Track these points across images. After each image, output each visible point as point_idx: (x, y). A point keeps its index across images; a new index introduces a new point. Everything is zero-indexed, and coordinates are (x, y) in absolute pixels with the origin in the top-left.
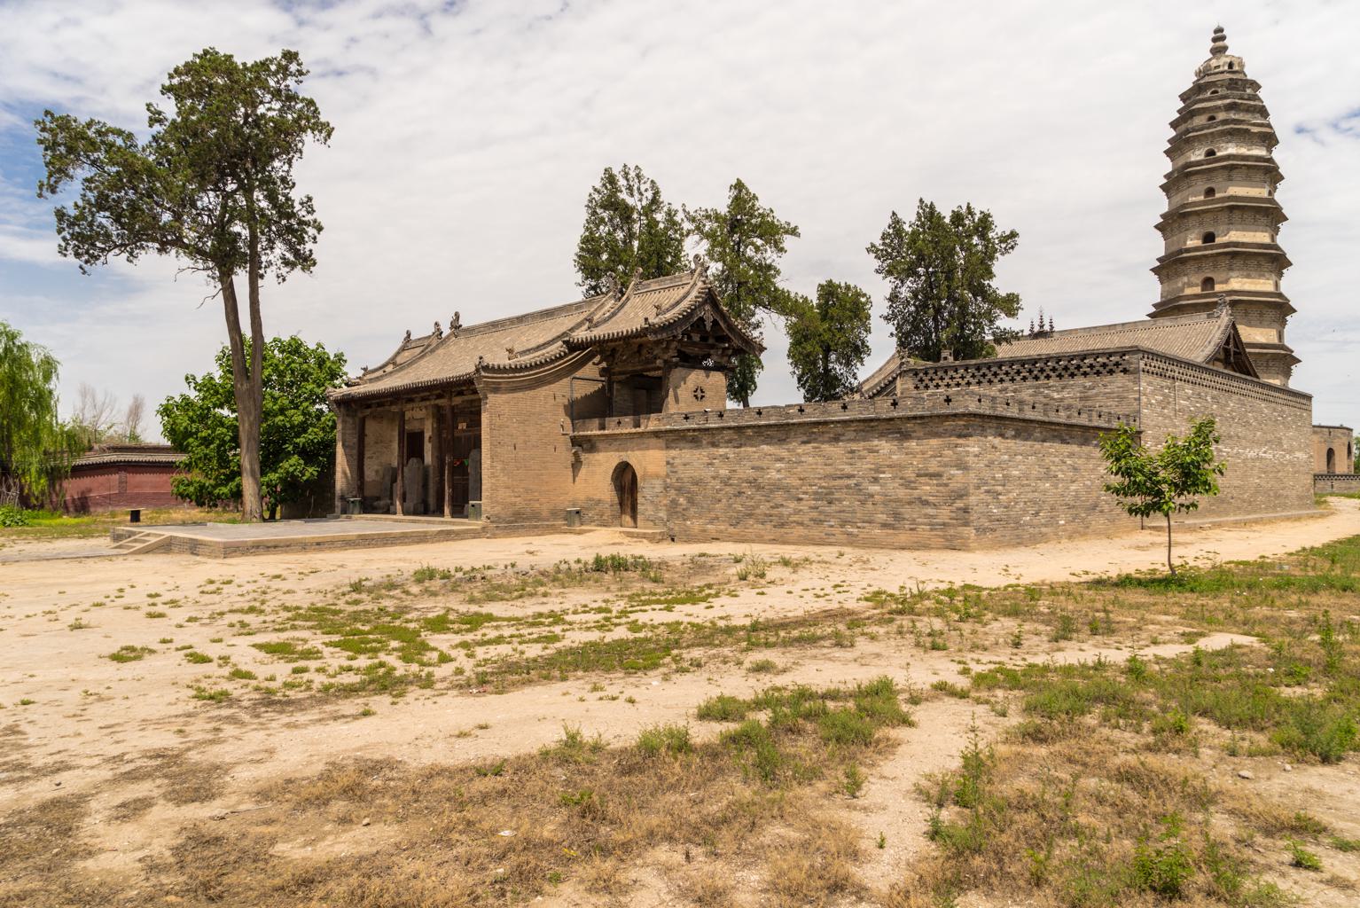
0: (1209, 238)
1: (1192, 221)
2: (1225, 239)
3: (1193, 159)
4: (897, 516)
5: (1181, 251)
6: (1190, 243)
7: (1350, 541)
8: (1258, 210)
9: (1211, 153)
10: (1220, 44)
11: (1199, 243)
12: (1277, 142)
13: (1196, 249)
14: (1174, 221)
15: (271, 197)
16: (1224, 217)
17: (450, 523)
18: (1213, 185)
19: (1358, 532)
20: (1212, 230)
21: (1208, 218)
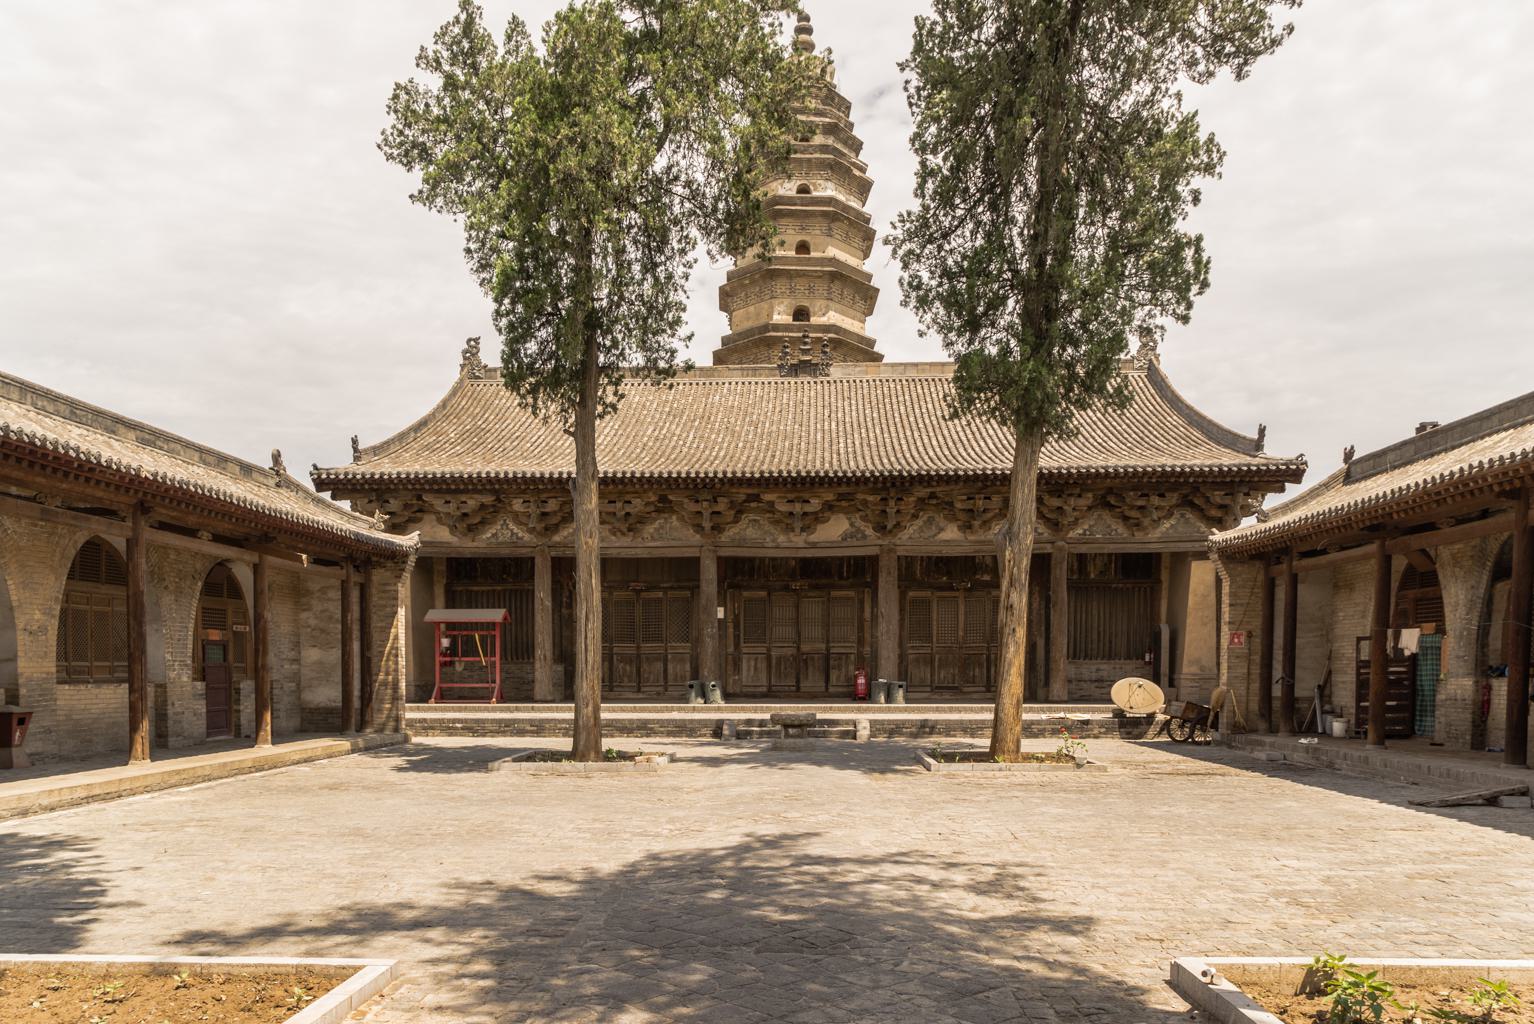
0: (801, 314)
1: (780, 286)
2: (823, 320)
3: (781, 192)
4: (663, 499)
5: (766, 328)
6: (777, 318)
7: (1522, 400)
8: (856, 282)
9: (803, 190)
10: (803, 37)
11: (788, 319)
12: (723, 338)
13: (786, 328)
14: (753, 282)
15: (1214, 886)
16: (821, 287)
17: (905, 710)
18: (807, 238)
19: (1531, 389)
20: (806, 303)
21: (801, 285)
